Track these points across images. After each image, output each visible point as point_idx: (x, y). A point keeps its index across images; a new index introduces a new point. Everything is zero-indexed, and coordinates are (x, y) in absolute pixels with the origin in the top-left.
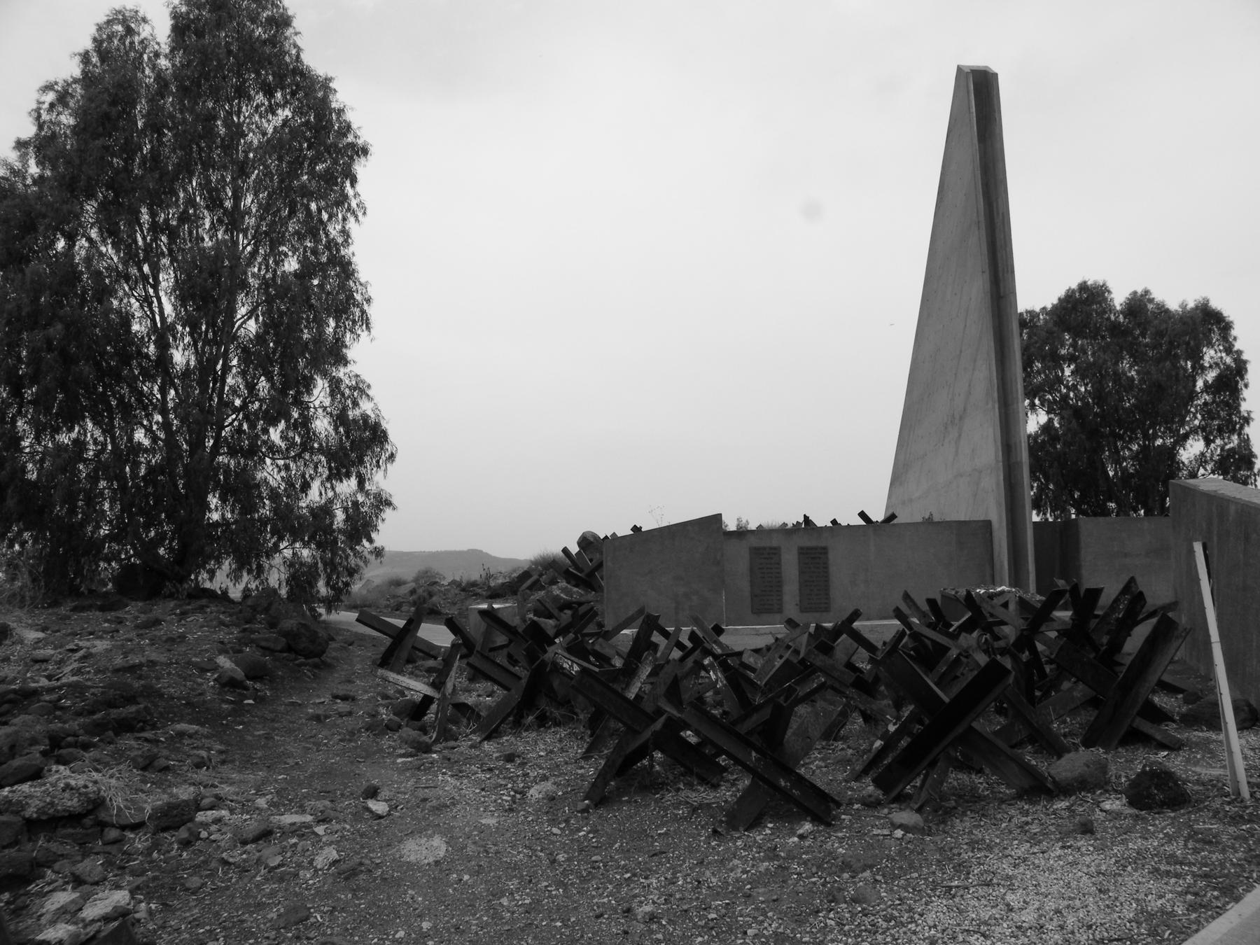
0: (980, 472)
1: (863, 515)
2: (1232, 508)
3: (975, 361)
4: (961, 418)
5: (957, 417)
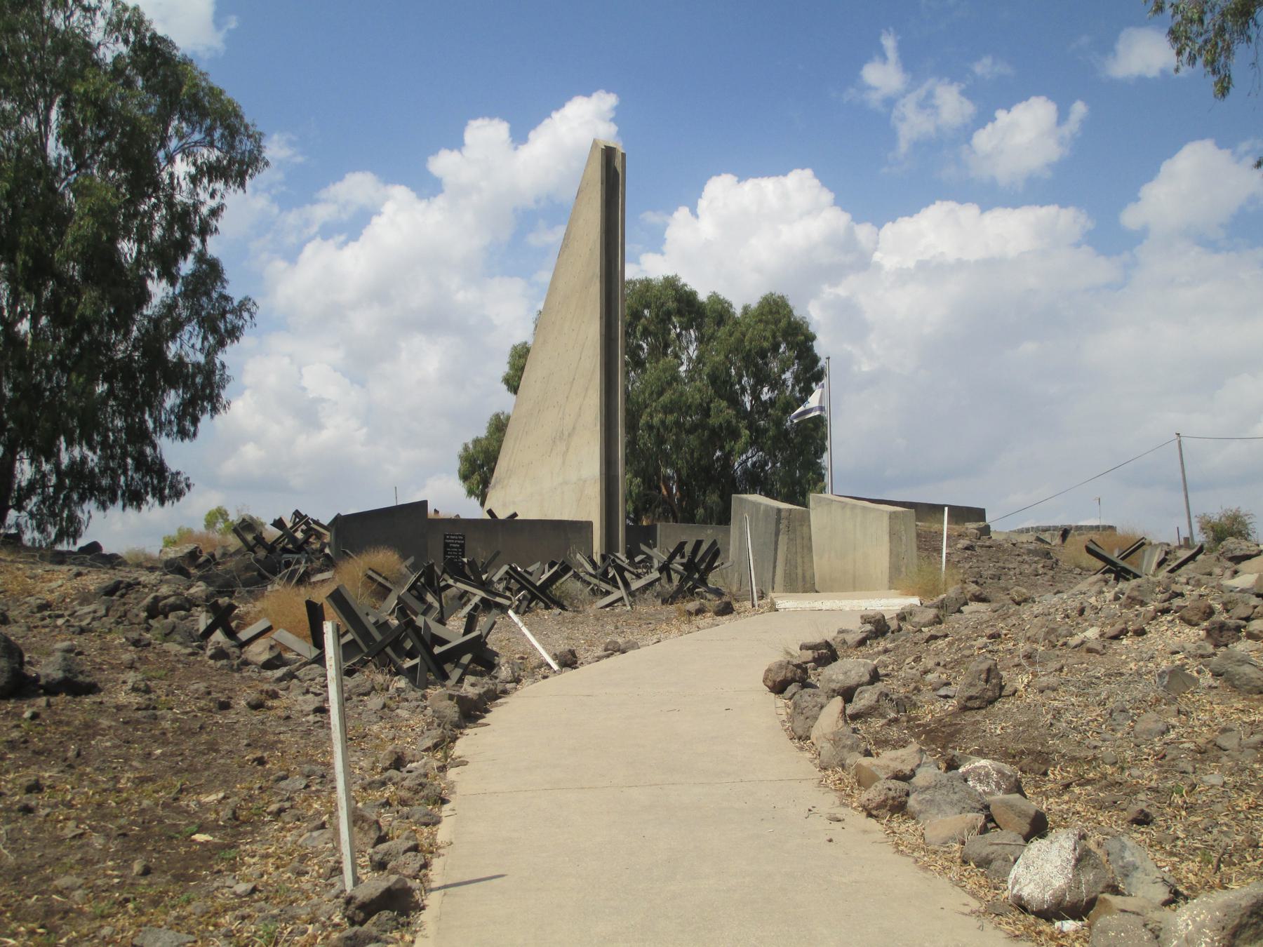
0: (585, 481)
2: (762, 508)
3: (587, 389)
4: (569, 435)
5: (566, 433)
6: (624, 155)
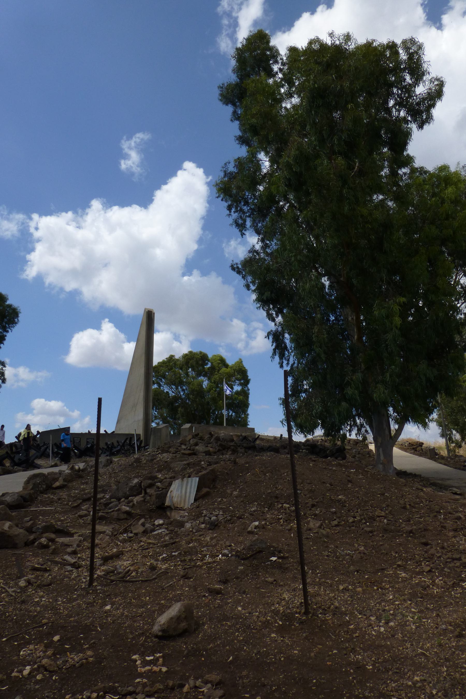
1: (105, 431)
6: (154, 313)
